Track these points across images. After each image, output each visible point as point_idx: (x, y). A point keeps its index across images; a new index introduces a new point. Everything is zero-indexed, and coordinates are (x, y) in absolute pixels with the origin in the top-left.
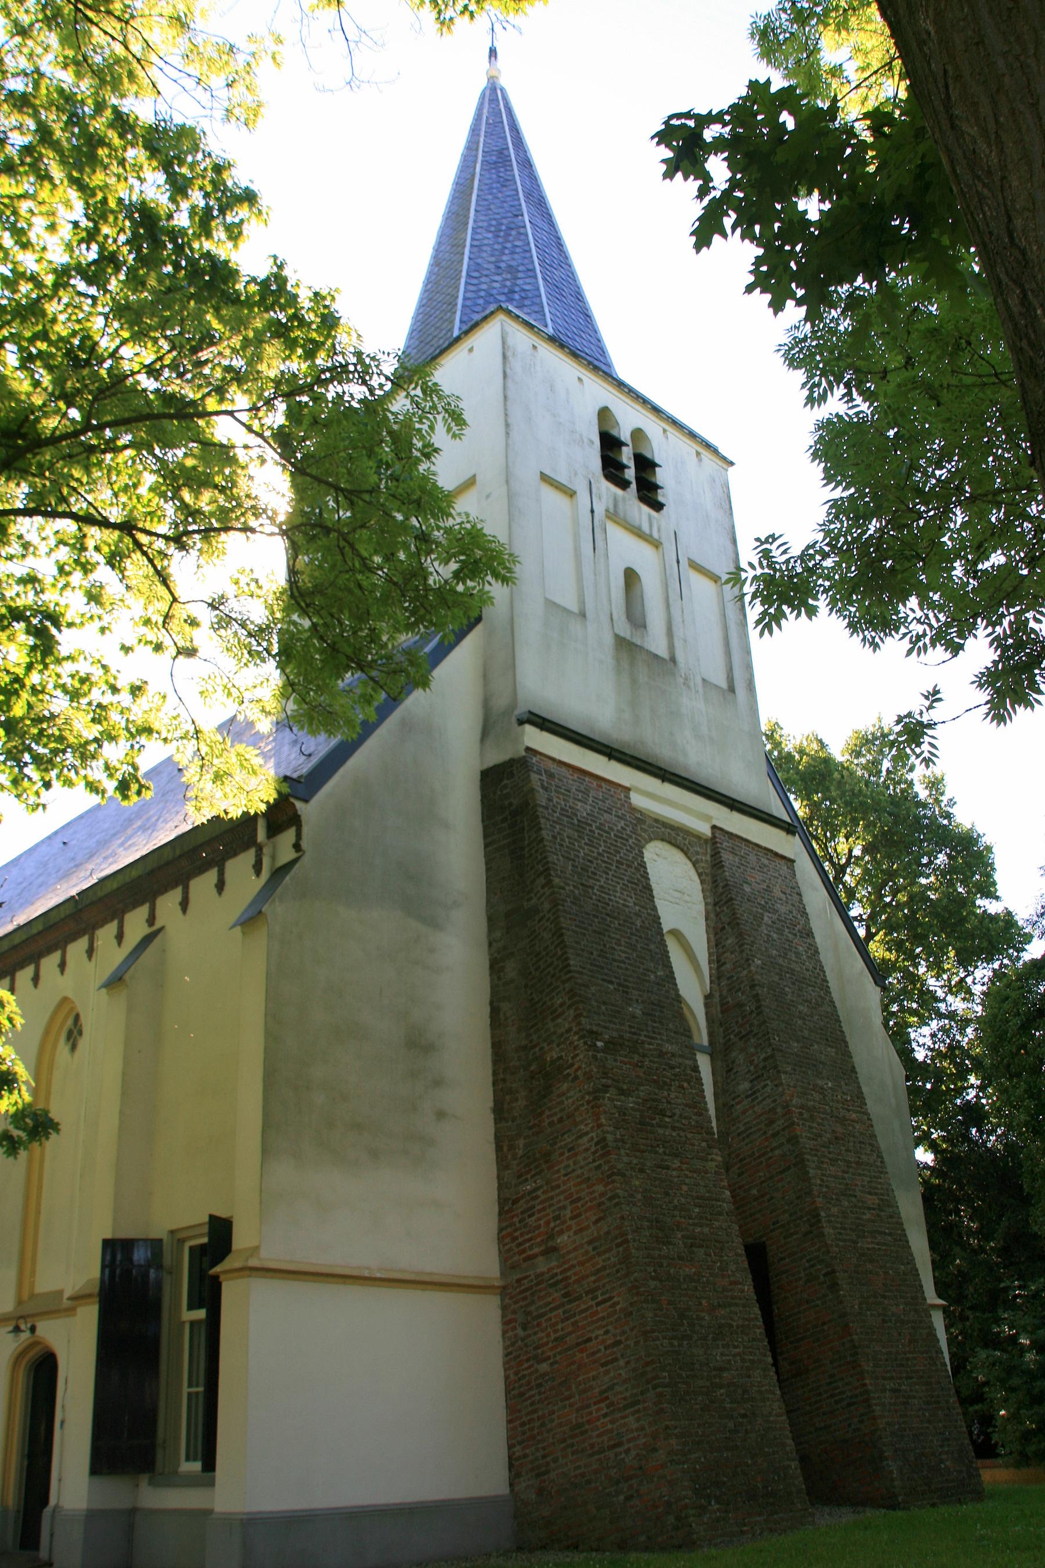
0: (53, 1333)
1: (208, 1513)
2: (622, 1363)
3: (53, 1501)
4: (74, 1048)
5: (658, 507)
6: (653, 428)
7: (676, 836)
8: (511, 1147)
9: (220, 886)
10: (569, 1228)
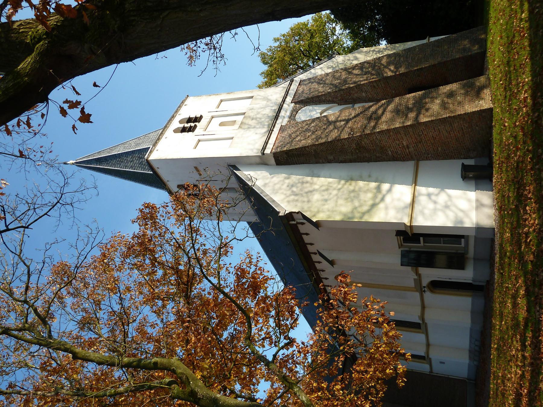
0: (425, 282)
1: (476, 237)
3: (471, 282)
5: (201, 117)
6: (178, 118)
7: (292, 116)
8: (379, 157)
9: (307, 234)
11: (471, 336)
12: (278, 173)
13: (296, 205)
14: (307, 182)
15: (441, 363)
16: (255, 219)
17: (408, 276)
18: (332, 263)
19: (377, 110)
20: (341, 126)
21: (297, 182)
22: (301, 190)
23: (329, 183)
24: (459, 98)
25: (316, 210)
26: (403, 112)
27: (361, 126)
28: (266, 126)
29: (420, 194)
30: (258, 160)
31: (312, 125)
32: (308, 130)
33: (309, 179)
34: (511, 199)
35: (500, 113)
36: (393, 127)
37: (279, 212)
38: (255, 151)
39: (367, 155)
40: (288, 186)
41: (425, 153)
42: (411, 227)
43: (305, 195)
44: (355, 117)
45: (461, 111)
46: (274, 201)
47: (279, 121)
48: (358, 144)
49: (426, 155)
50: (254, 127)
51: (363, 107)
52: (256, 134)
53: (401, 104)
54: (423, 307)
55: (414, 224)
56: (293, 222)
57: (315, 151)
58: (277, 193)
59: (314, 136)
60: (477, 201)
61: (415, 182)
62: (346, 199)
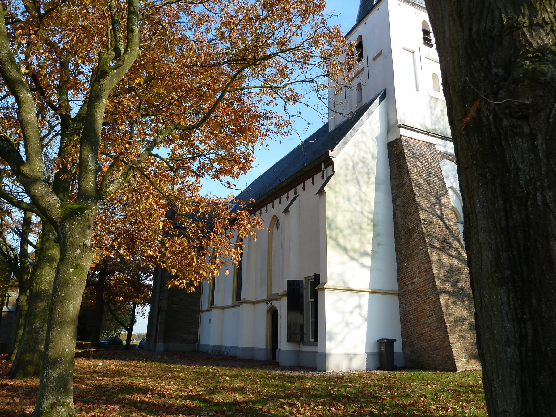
0: (276, 304)
2: (434, 316)
3: (279, 348)
4: (278, 229)
8: (401, 253)
9: (313, 183)
10: (418, 277)
11: (231, 347)
12: (378, 145)
13: (341, 168)
14: (369, 178)
15: (210, 320)
16: (331, 128)
17: (281, 288)
18: (286, 211)
19: (455, 249)
20: (434, 211)
21: (369, 167)
22: (359, 172)
23: (369, 202)
24: (469, 336)
25: (337, 190)
26: (452, 277)
27: (434, 233)
28: (433, 127)
29: (360, 297)
30: (392, 122)
31: (436, 179)
32: (429, 174)
33: (373, 179)
34: (342, 390)
35: (446, 380)
36: (433, 266)
37: (332, 150)
38: (403, 118)
39: (403, 240)
40: (363, 158)
41: (406, 301)
42: (323, 289)
43: (354, 176)
44: (446, 225)
45: (453, 338)
46: (345, 144)
47: (441, 141)
48: (414, 230)
49: (404, 302)
50: (432, 114)
51: (459, 233)
52: (424, 117)
53: (462, 274)
54: (254, 303)
55: (326, 292)
56: (323, 167)
57: (405, 184)
58: (355, 146)
59: (421, 181)
60: (355, 355)
61: (373, 292)
62: (351, 221)
